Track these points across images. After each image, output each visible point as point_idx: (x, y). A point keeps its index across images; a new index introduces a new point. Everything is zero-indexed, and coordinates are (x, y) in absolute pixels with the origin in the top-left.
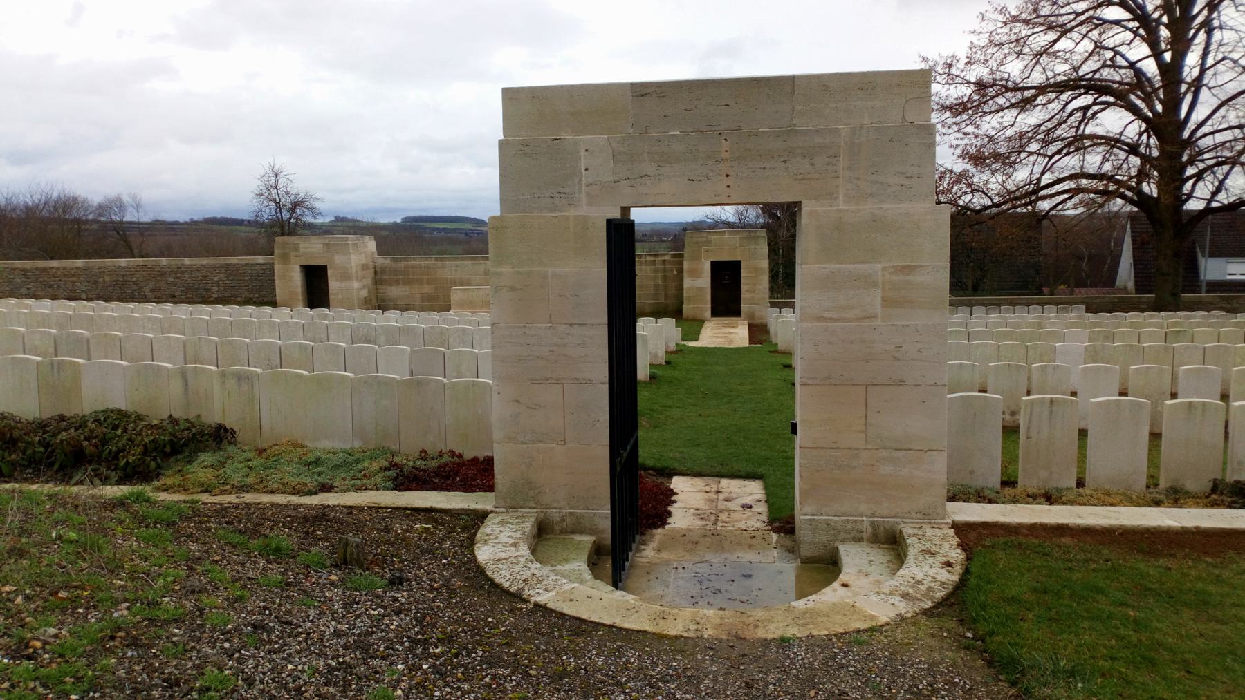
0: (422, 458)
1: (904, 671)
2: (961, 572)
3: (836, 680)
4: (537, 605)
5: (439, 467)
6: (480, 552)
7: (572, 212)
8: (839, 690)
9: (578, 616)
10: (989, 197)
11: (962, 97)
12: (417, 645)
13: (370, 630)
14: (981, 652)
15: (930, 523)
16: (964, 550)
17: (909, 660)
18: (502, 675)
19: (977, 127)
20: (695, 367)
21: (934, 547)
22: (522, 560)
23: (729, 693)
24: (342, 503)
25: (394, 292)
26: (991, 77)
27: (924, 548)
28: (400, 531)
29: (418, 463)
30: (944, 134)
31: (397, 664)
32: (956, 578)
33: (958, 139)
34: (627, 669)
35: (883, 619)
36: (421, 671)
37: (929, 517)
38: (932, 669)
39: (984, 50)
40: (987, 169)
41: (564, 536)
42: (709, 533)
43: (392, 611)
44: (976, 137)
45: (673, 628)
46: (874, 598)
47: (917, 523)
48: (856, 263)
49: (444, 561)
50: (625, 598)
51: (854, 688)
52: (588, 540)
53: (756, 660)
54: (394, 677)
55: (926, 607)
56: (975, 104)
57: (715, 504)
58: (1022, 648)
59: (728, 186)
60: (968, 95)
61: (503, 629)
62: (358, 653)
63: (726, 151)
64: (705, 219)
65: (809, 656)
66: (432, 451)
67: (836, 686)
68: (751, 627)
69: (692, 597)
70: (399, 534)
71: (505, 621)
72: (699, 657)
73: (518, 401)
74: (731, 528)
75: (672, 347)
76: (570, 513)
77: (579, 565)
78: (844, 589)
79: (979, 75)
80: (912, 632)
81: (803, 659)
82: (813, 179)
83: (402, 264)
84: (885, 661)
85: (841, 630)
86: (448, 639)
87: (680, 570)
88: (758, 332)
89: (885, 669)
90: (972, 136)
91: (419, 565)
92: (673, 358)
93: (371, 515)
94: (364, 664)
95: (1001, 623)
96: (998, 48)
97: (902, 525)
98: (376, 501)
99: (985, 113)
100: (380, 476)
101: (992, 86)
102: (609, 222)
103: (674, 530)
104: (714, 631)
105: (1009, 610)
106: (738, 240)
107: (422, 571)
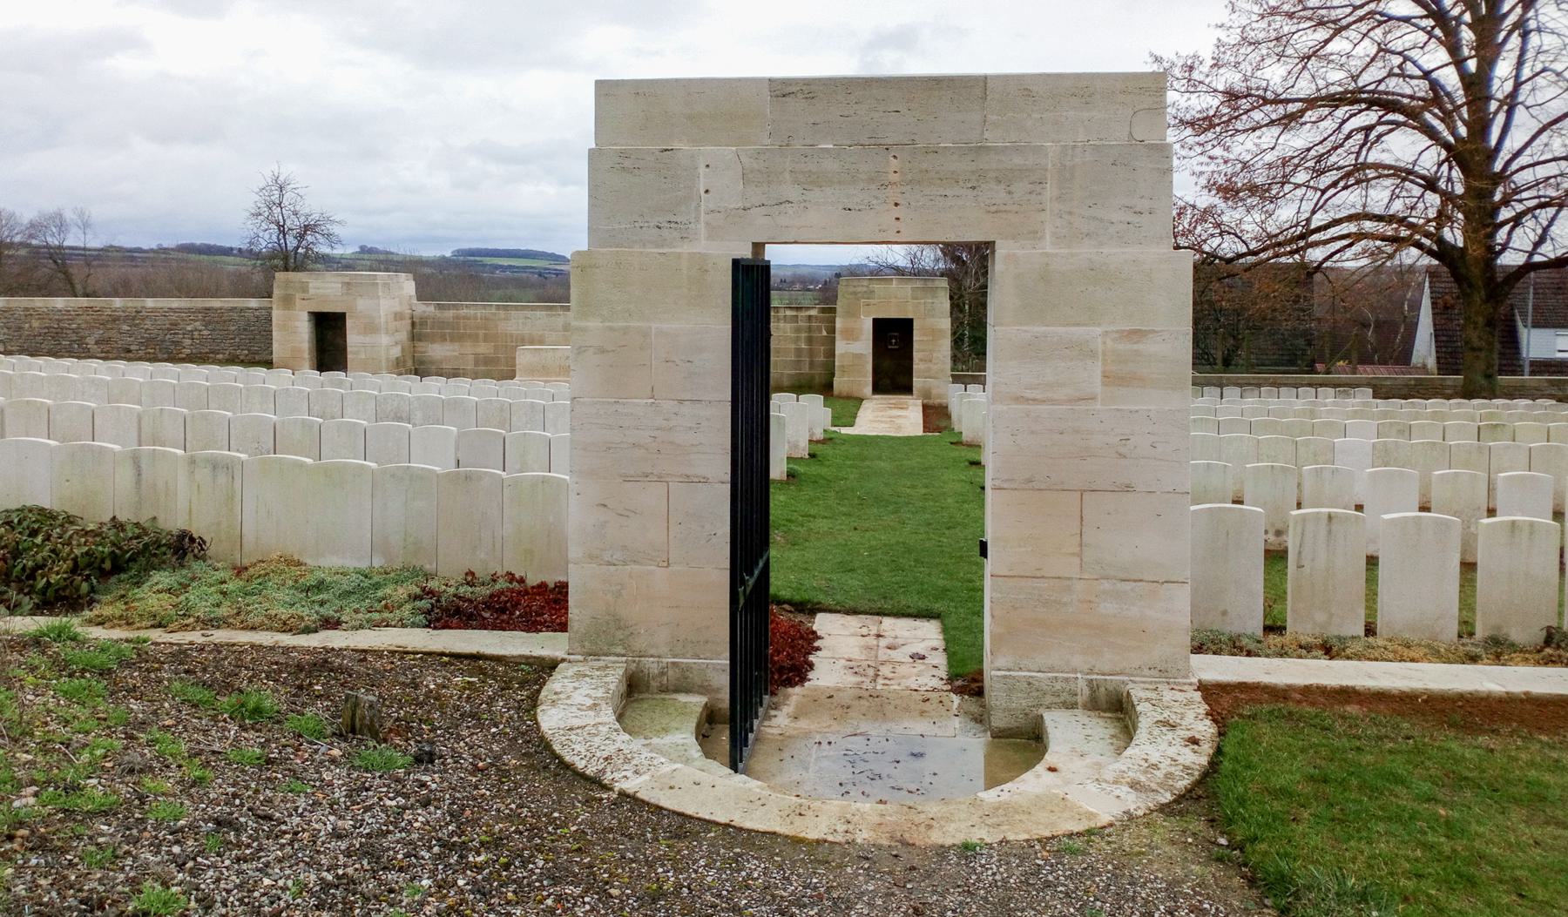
0: (468, 583)
1: (1134, 892)
2: (1211, 752)
4: (623, 794)
5: (492, 596)
7: (685, 249)
12: (451, 850)
13: (384, 828)
15: (1168, 683)
16: (1214, 720)
18: (571, 895)
19: (1227, 149)
20: (848, 462)
21: (1174, 717)
22: (604, 729)
24: (352, 646)
25: (437, 351)
26: (1244, 84)
27: (1161, 718)
29: (462, 590)
30: (1184, 158)
32: (1204, 760)
34: (748, 887)
36: (455, 888)
37: (1166, 674)
39: (1235, 50)
40: (1240, 204)
41: (663, 696)
46: (1092, 788)
47: (1151, 682)
49: (494, 730)
52: (697, 701)
54: (416, 898)
55: (1164, 801)
56: (1224, 119)
57: (873, 653)
59: (898, 219)
60: (1214, 107)
62: (365, 862)
63: (895, 172)
68: (922, 829)
69: (841, 784)
70: (431, 691)
71: (577, 817)
73: (605, 506)
74: (896, 687)
75: (819, 435)
76: (673, 663)
77: (684, 737)
78: (1052, 774)
79: (1229, 82)
80: (1145, 837)
81: (994, 874)
82: (1010, 212)
83: (450, 313)
84: (1108, 878)
85: (1048, 834)
86: (496, 843)
87: (825, 745)
88: (936, 415)
89: (1107, 889)
90: (1220, 161)
91: (458, 735)
92: (819, 449)
93: (392, 663)
94: (374, 878)
96: (1253, 47)
97: (1131, 685)
99: (1237, 131)
100: (406, 610)
101: (1246, 97)
102: (736, 263)
103: (816, 689)
104: (872, 833)
105: (1277, 806)
107: (462, 744)
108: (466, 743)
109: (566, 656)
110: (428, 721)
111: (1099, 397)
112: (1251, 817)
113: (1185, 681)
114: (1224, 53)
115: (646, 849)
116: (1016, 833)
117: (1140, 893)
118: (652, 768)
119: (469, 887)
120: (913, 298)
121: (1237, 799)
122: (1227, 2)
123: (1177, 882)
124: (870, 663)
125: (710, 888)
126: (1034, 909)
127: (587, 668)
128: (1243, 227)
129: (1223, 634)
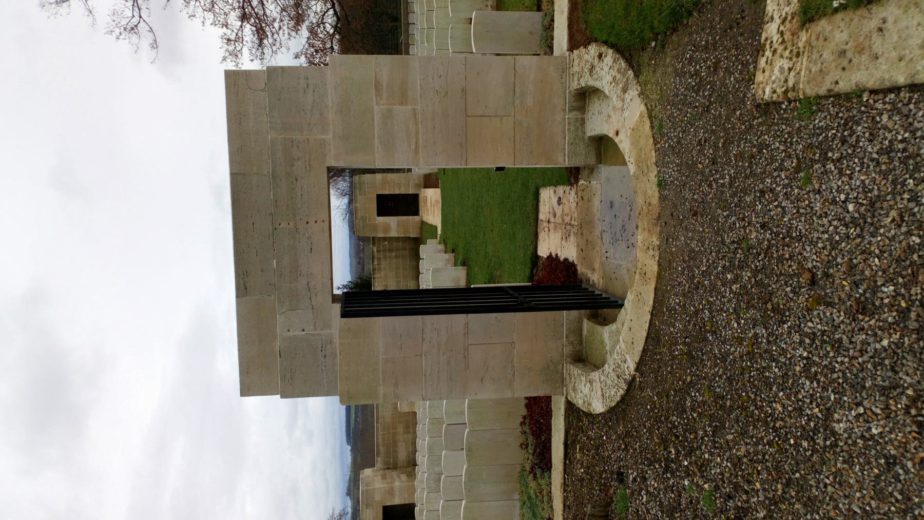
0: (527, 448)
1: (682, 95)
2: (605, 47)
3: (690, 147)
4: (637, 370)
5: (533, 435)
6: (597, 409)
7: (337, 341)
8: (697, 145)
9: (644, 339)
10: (327, 11)
11: (252, 31)
12: (669, 467)
13: (658, 503)
14: (666, 36)
15: (569, 68)
16: (589, 44)
17: (674, 91)
18: (691, 403)
19: (274, 20)
20: (456, 232)
21: (587, 66)
22: (603, 378)
23: (701, 229)
24: (561, 512)
25: (402, 455)
26: (237, 10)
27: (588, 73)
28: (582, 470)
29: (531, 451)
30: (281, 44)
31: (684, 485)
32: (610, 51)
33: (284, 34)
34: (684, 305)
35: (643, 108)
36: (689, 466)
37: (564, 68)
38: (680, 74)
39: (217, 15)
40: (306, 13)
41: (584, 342)
42: (580, 231)
43: (643, 483)
44: (282, 21)
45: (653, 268)
46: (626, 114)
47: (569, 78)
48: (373, 126)
49: (605, 438)
50: (630, 300)
51: (695, 134)
52: (586, 325)
53: (675, 206)
54: (695, 488)
55: (632, 75)
56: (257, 21)
57: (558, 225)
58: (662, 6)
59: (316, 222)
60: (251, 27)
61: (656, 398)
62: (677, 515)
63: (289, 224)
64: (346, 220)
65: (671, 167)
66: (522, 440)
67: (694, 147)
68: (651, 208)
69: (628, 247)
70: (585, 471)
71: (650, 395)
72: (674, 249)
73: (482, 379)
74: (576, 214)
75: (442, 247)
76: (567, 337)
77: (606, 332)
78: (620, 134)
79: (236, 18)
80: (652, 86)
81: (674, 171)
82: (310, 159)
83: (381, 448)
84: (675, 109)
85: (652, 140)
86: (664, 442)
87: (608, 255)
88: (430, 181)
89: (680, 110)
90: (281, 24)
91: (608, 457)
92: (450, 247)
93: (570, 491)
94: (684, 511)
95: (644, 20)
96: (215, 5)
97: (571, 89)
98: (560, 486)
99: (264, 15)
100: (542, 482)
101: (244, 9)
102: (344, 315)
103: (578, 257)
104: (654, 236)
105: (634, 13)
106: (362, 196)
107: (612, 456)
108: (612, 453)
109: (564, 396)
110: (601, 473)
111: (413, 107)
112: (640, 28)
113: (568, 59)
114: (219, 21)
115: (666, 359)
116: (652, 157)
117: (682, 92)
118: (622, 353)
119: (688, 459)
120: (365, 195)
121: (631, 35)
122: (189, 20)
123: (676, 70)
124: (563, 228)
125: (685, 326)
126: (692, 150)
127: (570, 385)
128: (319, 10)
129: (542, 34)
